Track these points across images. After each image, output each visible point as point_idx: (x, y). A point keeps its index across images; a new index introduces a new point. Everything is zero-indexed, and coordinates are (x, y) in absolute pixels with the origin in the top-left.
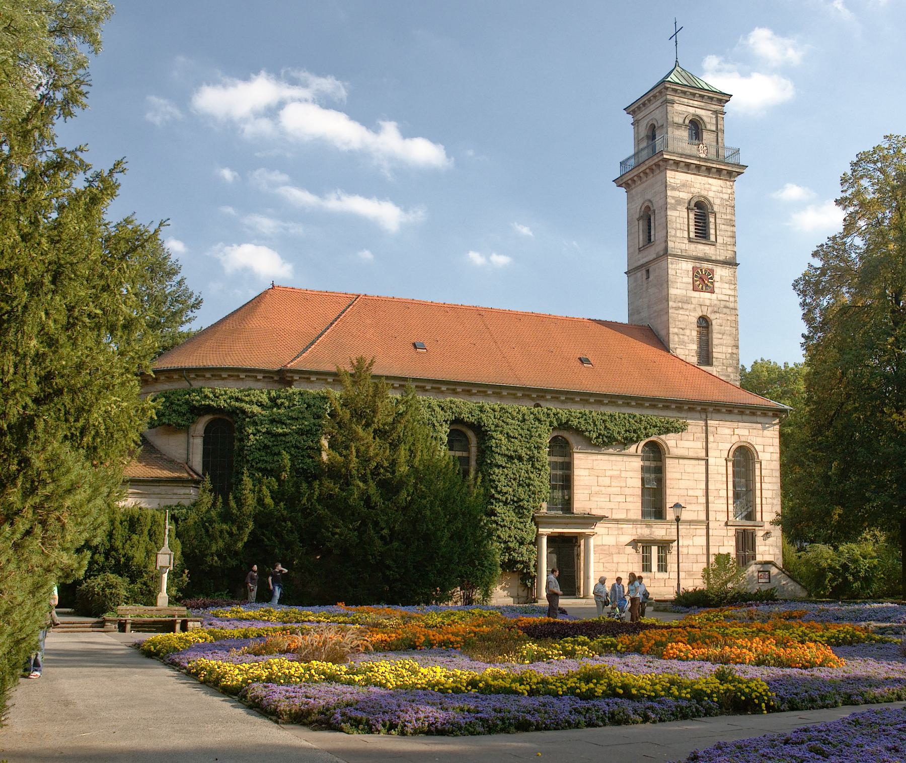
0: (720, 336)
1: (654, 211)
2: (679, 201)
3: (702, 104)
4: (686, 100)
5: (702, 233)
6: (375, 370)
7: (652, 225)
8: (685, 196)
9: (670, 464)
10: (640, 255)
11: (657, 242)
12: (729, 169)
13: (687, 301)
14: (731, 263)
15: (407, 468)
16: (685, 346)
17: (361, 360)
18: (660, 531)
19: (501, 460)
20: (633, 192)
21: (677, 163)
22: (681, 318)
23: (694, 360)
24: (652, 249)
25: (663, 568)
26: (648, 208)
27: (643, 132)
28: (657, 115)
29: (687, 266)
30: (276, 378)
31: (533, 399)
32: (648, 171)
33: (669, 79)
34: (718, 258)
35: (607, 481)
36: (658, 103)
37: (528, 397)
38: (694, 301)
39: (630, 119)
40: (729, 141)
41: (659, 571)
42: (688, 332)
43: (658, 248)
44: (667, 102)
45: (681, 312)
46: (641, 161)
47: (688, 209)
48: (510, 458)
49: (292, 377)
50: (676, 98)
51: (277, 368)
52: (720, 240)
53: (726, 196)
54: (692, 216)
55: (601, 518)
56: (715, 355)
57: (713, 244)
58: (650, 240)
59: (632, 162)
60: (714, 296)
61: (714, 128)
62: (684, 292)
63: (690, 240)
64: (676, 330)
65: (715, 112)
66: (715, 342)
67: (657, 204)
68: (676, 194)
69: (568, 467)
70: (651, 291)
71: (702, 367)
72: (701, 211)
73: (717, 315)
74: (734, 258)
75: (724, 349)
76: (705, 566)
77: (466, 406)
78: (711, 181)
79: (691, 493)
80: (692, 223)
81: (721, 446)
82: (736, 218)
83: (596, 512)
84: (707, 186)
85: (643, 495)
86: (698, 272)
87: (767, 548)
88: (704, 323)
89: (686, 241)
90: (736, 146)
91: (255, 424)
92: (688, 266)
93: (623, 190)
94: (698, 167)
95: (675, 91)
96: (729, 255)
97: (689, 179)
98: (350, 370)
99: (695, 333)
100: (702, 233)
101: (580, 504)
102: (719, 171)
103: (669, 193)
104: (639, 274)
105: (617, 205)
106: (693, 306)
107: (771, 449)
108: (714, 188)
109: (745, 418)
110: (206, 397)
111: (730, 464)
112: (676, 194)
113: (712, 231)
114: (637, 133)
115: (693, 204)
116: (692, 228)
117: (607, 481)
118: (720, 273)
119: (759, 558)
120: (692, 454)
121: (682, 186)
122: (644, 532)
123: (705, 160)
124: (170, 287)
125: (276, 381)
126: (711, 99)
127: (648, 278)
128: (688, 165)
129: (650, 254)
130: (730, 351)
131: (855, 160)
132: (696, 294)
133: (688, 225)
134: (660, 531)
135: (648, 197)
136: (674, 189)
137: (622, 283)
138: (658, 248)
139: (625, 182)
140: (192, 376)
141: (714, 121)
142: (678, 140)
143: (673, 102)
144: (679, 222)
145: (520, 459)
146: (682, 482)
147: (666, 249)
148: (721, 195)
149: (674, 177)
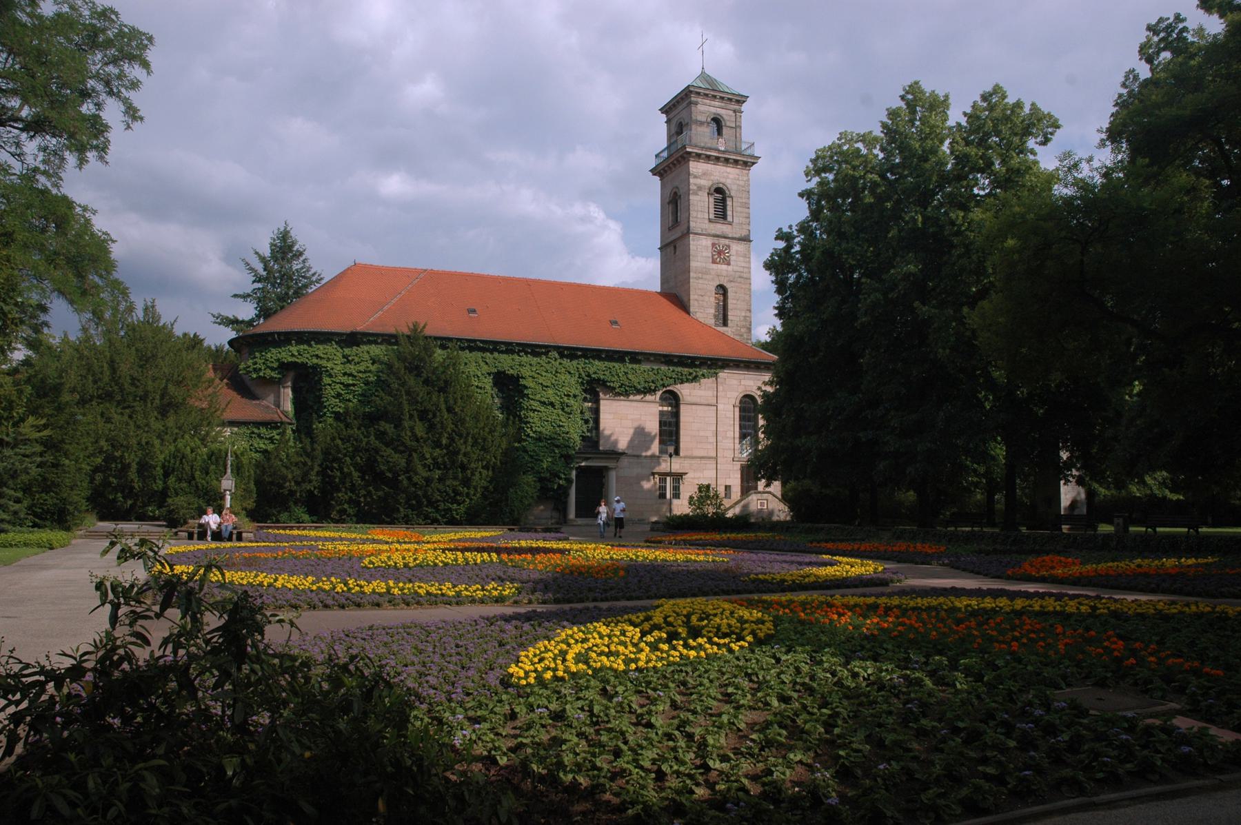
2: (700, 188)
5: (721, 213)
6: (427, 332)
9: (682, 408)
13: (705, 272)
14: (746, 239)
16: (703, 307)
17: (415, 325)
19: (535, 405)
21: (699, 156)
23: (711, 321)
27: (673, 130)
28: (684, 114)
29: (707, 242)
36: (685, 104)
39: (664, 117)
40: (747, 134)
42: (706, 298)
43: (683, 228)
44: (690, 103)
48: (543, 403)
51: (348, 331)
53: (742, 183)
54: (712, 200)
57: (730, 224)
59: (665, 154)
60: (730, 268)
63: (710, 221)
65: (735, 111)
67: (681, 192)
68: (698, 181)
69: (596, 412)
72: (720, 194)
75: (738, 313)
77: (506, 362)
78: (729, 170)
79: (702, 434)
80: (712, 206)
81: (729, 394)
82: (751, 201)
88: (722, 290)
91: (330, 376)
92: (707, 242)
94: (717, 158)
95: (699, 94)
96: (744, 233)
98: (407, 332)
99: (713, 299)
100: (721, 213)
102: (736, 162)
103: (692, 180)
105: (652, 192)
110: (293, 355)
111: (737, 410)
112: (698, 181)
114: (669, 130)
116: (712, 210)
118: (736, 247)
121: (702, 174)
123: (724, 152)
124: (296, 265)
126: (730, 100)
131: (813, 157)
132: (714, 266)
136: (696, 177)
138: (683, 228)
139: (660, 171)
142: (701, 136)
143: (696, 103)
144: (700, 207)
145: (552, 404)
147: (689, 228)
149: (696, 167)
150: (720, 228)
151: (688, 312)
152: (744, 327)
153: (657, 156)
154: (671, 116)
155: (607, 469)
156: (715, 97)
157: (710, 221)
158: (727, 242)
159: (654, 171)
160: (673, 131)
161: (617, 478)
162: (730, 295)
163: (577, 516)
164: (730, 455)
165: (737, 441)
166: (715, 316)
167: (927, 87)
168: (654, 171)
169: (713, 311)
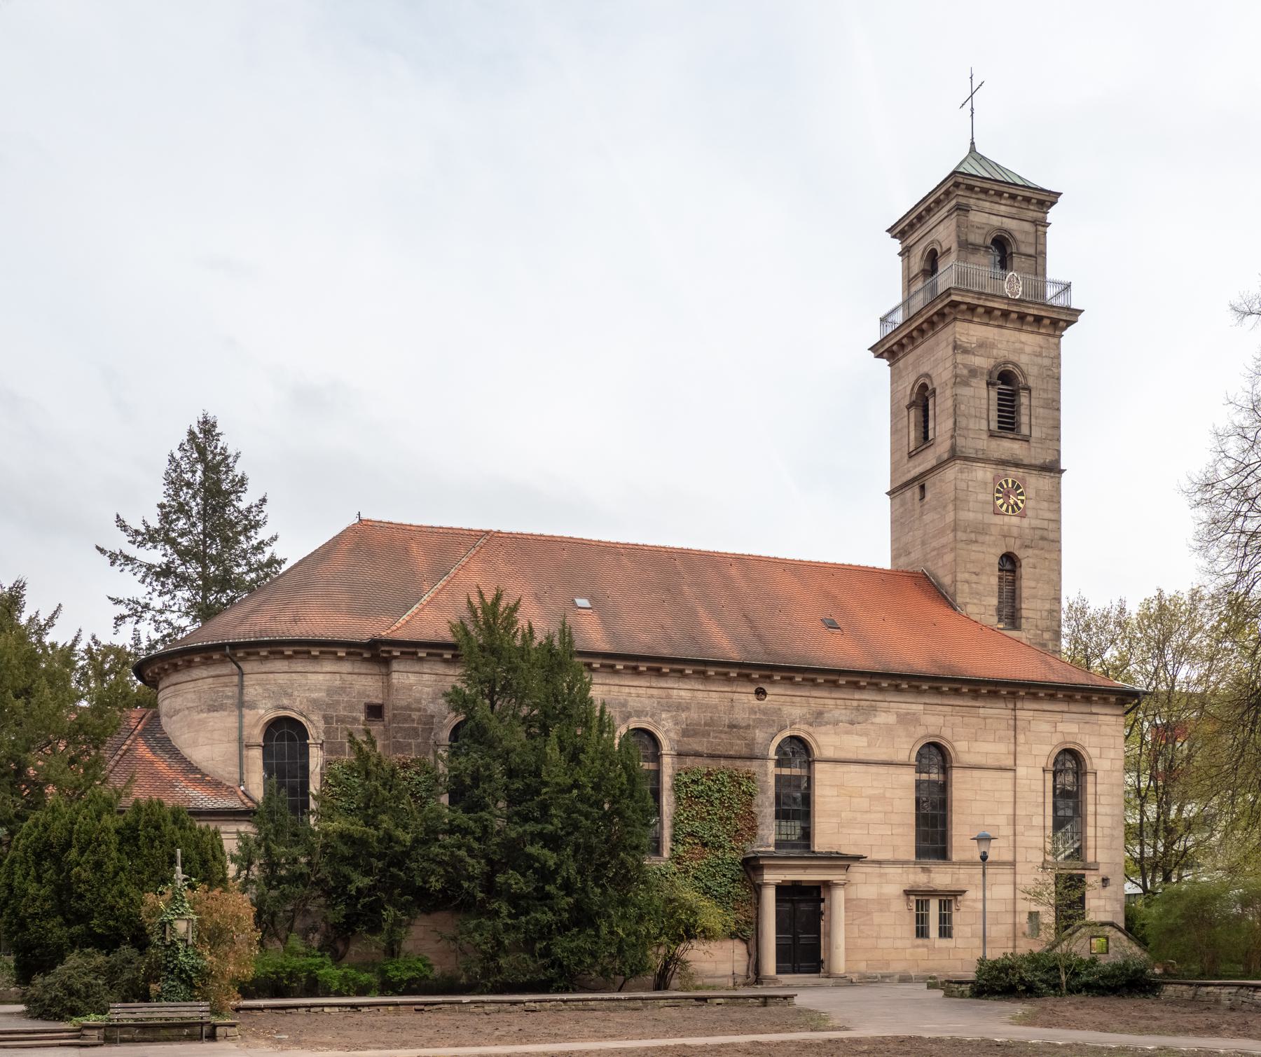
0: (1033, 584)
1: (934, 391)
3: (1014, 210)
4: (987, 204)
7: (931, 413)
8: (982, 362)
9: (956, 775)
10: (911, 464)
11: (939, 440)
12: (1054, 316)
15: (497, 828)
18: (941, 877)
20: (901, 364)
21: (972, 309)
22: (974, 556)
24: (932, 450)
25: (945, 932)
26: (924, 387)
27: (917, 264)
30: (366, 655)
31: (752, 681)
32: (925, 326)
33: (961, 170)
34: (1033, 462)
35: (864, 804)
37: (747, 678)
38: (994, 530)
39: (897, 245)
41: (940, 936)
42: (984, 579)
45: (974, 547)
46: (914, 311)
47: (988, 384)
49: (389, 652)
50: (972, 201)
52: (1036, 433)
54: (994, 395)
55: (858, 858)
56: (1024, 613)
57: (1026, 439)
58: (926, 437)
59: (899, 318)
60: (1025, 522)
61: (1031, 251)
62: (980, 516)
64: (966, 576)
66: (1025, 593)
70: (927, 518)
71: (1005, 632)
72: (1007, 383)
73: (1030, 552)
74: (1058, 461)
75: (1038, 604)
76: (1010, 927)
78: (1024, 337)
83: (846, 851)
84: (1018, 345)
85: (917, 825)
86: (1001, 485)
87: (1102, 902)
88: (1009, 562)
89: (985, 436)
90: (1066, 280)
93: (884, 363)
95: (970, 188)
97: (991, 336)
99: (994, 581)
100: (1008, 422)
101: (821, 842)
102: (1038, 320)
104: (908, 494)
106: (993, 538)
107: (1112, 754)
108: (1028, 349)
109: (1074, 707)
113: (1024, 419)
114: (907, 268)
115: (996, 374)
116: (994, 415)
117: (864, 804)
118: (1036, 483)
119: (1091, 917)
120: (991, 762)
122: (918, 878)
125: (366, 660)
126: (1027, 200)
127: (923, 497)
128: (989, 311)
129: (928, 459)
130: (1047, 606)
132: (997, 520)
133: (988, 410)
134: (941, 877)
135: (924, 369)
137: (883, 508)
139: (891, 349)
140: (240, 654)
141: (1031, 239)
146: (975, 805)
148: (1039, 360)
150: (1008, 447)
151: (952, 606)
152: (1048, 629)
153: (883, 320)
154: (911, 241)
155: (828, 885)
156: (999, 194)
157: (992, 435)
158: (1020, 472)
159: (879, 350)
160: (916, 269)
161: (847, 901)
162: (1026, 571)
163: (779, 971)
164: (1038, 858)
165: (1049, 832)
166: (999, 610)
167: (1053, 215)
168: (879, 350)
169: (995, 601)
